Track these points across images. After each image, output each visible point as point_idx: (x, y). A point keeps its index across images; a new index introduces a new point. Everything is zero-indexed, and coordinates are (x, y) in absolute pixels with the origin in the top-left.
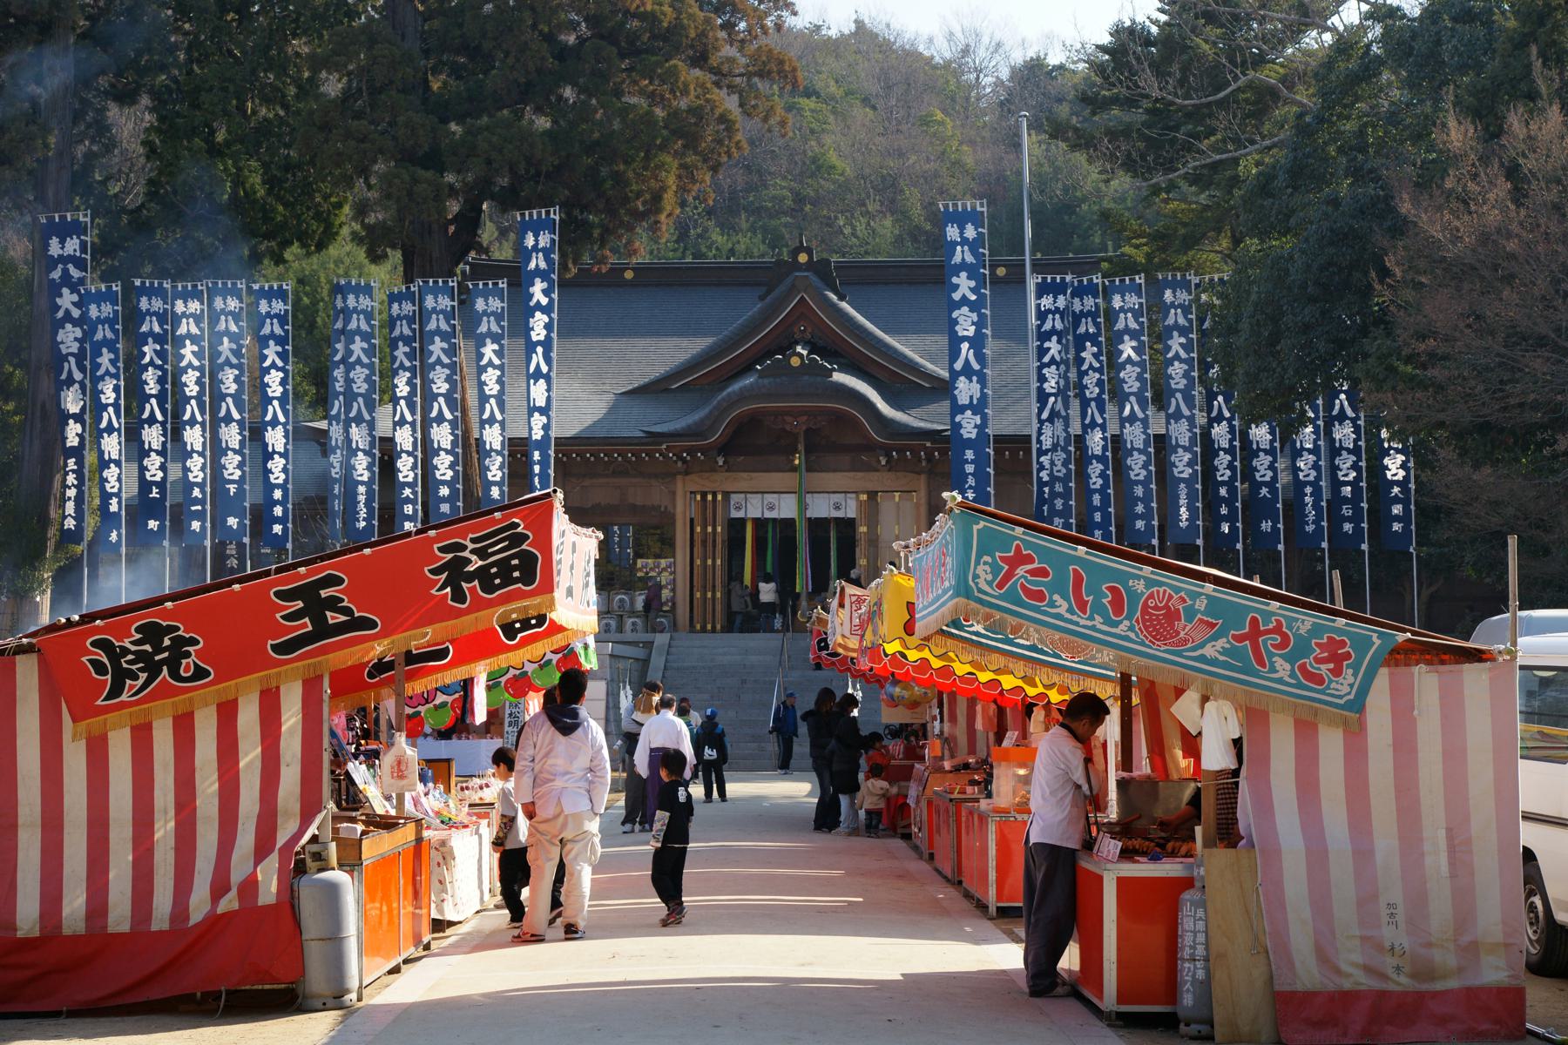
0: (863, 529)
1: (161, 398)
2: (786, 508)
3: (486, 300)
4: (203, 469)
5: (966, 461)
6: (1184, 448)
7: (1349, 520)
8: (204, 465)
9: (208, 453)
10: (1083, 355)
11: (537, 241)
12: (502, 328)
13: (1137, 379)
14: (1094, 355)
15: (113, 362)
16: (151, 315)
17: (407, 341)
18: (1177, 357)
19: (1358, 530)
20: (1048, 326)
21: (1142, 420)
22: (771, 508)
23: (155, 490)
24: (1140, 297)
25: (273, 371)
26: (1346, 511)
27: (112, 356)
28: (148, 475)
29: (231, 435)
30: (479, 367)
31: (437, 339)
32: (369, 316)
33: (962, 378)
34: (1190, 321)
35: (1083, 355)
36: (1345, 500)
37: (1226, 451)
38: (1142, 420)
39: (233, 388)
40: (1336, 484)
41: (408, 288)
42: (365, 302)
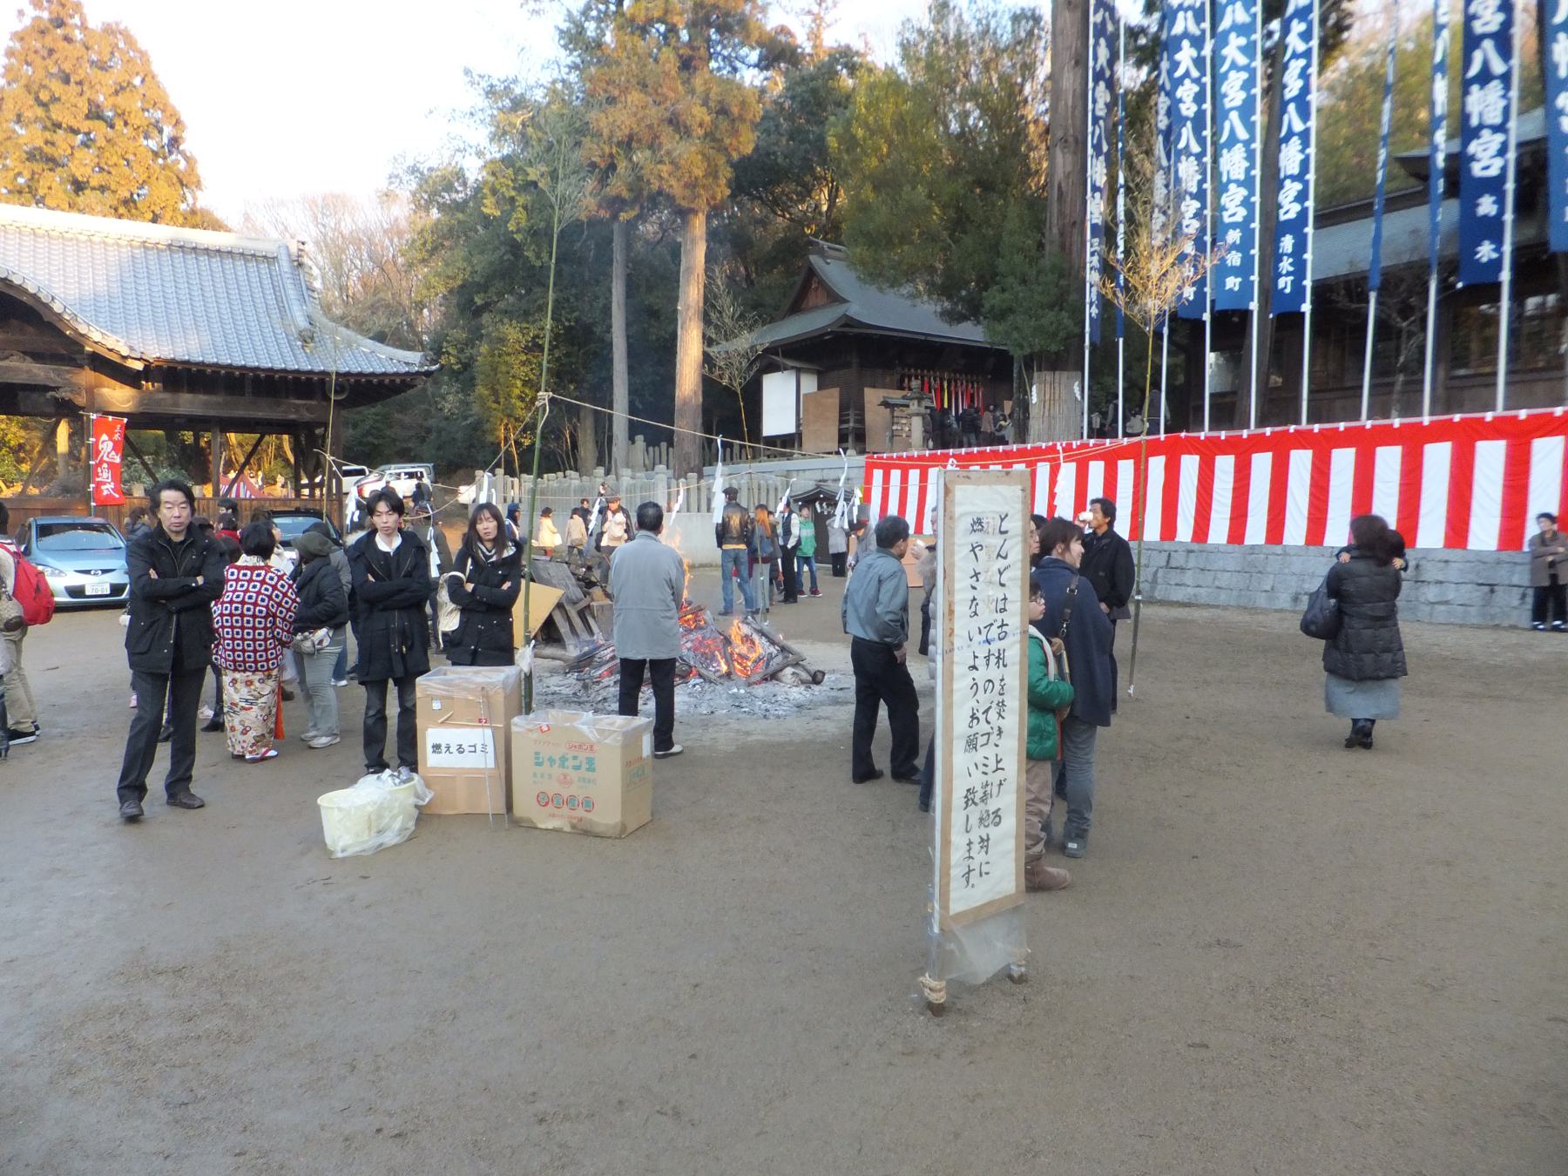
19: (1246, 286)
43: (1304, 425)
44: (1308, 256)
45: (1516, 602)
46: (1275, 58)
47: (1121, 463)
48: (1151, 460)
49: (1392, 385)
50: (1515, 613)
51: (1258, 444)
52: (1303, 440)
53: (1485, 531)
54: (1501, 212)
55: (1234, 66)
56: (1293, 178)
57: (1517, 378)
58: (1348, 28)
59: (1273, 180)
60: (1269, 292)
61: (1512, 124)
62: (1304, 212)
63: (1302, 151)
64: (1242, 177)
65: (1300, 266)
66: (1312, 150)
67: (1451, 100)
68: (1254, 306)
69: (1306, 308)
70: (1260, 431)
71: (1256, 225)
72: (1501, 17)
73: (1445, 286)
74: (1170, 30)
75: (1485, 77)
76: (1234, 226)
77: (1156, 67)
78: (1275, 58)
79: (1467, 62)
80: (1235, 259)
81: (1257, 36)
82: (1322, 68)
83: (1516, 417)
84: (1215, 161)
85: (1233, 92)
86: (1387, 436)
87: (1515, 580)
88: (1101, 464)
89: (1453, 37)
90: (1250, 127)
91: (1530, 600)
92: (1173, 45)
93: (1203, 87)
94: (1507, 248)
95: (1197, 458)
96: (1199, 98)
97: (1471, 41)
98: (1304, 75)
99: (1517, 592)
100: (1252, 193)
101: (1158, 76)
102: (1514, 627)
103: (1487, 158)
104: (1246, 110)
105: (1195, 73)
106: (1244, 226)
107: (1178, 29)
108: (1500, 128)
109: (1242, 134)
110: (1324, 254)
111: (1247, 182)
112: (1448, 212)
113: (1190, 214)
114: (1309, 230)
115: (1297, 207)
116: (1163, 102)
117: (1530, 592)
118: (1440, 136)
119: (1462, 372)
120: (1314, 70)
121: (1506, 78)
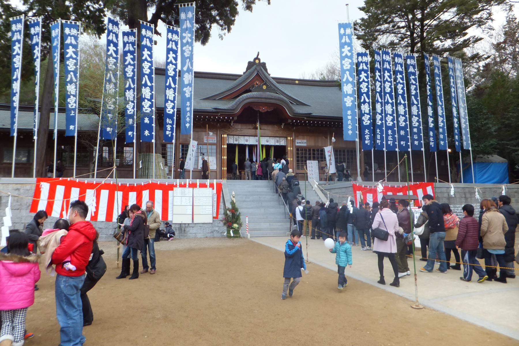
0: (289, 148)
2: (251, 141)
4: (133, 108)
5: (348, 115)
7: (416, 140)
8: (134, 106)
9: (135, 101)
10: (126, 58)
11: (345, 32)
12: (368, 67)
14: (131, 59)
19: (420, 144)
20: (127, 49)
21: (150, 87)
23: (73, 112)
24: (135, 38)
25: (129, 66)
26: (416, 137)
29: (401, 110)
30: (124, 65)
31: (70, 47)
33: (187, 74)
34: (135, 49)
35: (126, 58)
36: (415, 133)
38: (150, 87)
40: (411, 127)
41: (132, 31)
48: (144, 192)
55: (364, 81)
57: (79, 168)
59: (411, 116)
62: (174, 111)
63: (151, 92)
68: (384, 149)
71: (421, 127)
84: (385, 107)
90: (417, 101)
95: (108, 191)
100: (420, 119)
111: (418, 116)
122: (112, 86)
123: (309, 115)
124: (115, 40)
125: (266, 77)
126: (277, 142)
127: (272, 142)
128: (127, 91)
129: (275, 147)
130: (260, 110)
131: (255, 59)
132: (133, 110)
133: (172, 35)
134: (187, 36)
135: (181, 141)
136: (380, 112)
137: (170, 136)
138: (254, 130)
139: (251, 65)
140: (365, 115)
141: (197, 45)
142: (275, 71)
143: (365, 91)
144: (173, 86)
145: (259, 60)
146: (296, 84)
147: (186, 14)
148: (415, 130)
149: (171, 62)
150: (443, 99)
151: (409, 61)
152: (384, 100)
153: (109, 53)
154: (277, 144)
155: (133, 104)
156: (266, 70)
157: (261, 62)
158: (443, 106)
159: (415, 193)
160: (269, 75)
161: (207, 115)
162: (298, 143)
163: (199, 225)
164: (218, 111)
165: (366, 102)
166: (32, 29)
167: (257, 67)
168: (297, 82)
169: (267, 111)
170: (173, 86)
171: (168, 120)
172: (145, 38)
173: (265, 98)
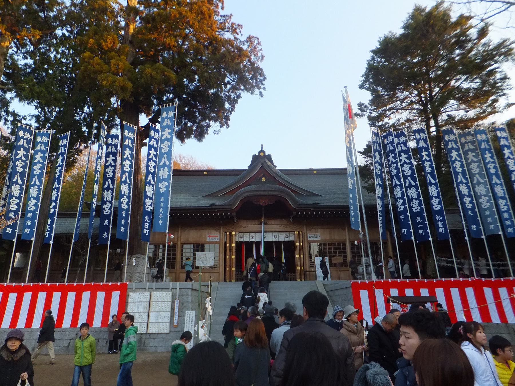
0: (297, 244)
1: (464, 173)
2: (257, 237)
3: (42, 138)
6: (415, 199)
11: (167, 115)
13: (410, 169)
14: (113, 160)
15: (492, 157)
16: (451, 141)
17: (472, 151)
18: (472, 161)
19: (32, 232)
21: (414, 186)
22: (252, 238)
25: (110, 167)
27: (490, 155)
28: (414, 209)
32: (456, 142)
34: (65, 150)
37: (468, 196)
39: (477, 170)
42: (452, 137)
43: (458, 278)
44: (54, 226)
45: (104, 345)
46: (53, 163)
47: (99, 293)
49: (77, 270)
50: (104, 348)
51: (27, 289)
52: (43, 288)
53: (97, 323)
54: (109, 224)
56: (400, 198)
58: (76, 163)
59: (28, 198)
60: (40, 234)
61: (113, 202)
62: (55, 211)
63: (416, 191)
64: (18, 196)
65: (51, 228)
66: (59, 194)
67: (99, 191)
69: (51, 242)
70: (11, 284)
71: (38, 212)
72: (112, 174)
73: (94, 243)
74: (17, 143)
75: (108, 189)
76: (31, 212)
77: (11, 152)
78: (53, 163)
79: (104, 184)
80: (29, 223)
81: (47, 155)
82: (66, 171)
83: (510, 280)
85: (37, 169)
86: (71, 288)
87: (105, 337)
88: (103, 293)
89: (100, 174)
90: (41, 181)
91: (108, 343)
92: (19, 148)
93: (132, 163)
94: (110, 235)
96: (24, 167)
97: (105, 179)
98: (60, 172)
99: (105, 341)
101: (12, 155)
102: (103, 353)
103: (107, 209)
104: (40, 176)
105: (459, 159)
106: (34, 212)
107: (21, 143)
108: (110, 202)
109: (38, 183)
110: (55, 227)
111: (37, 198)
112: (96, 222)
113: (467, 202)
114: (55, 218)
115: (403, 207)
116: (11, 164)
117: (108, 341)
118: (95, 200)
119: (99, 269)
120: (63, 171)
121: (113, 190)
122: (413, 189)
123: (316, 206)
124: (155, 145)
125: (271, 169)
126: (287, 237)
127: (281, 238)
128: (106, 191)
129: (285, 243)
130: (261, 204)
131: (260, 152)
132: (110, 211)
133: (419, 134)
134: (166, 134)
135: (182, 240)
136: (4, 197)
137: (147, 235)
138: (259, 226)
139: (255, 158)
140: (414, 200)
141: (176, 142)
142: (282, 162)
143: (111, 176)
144: (413, 184)
145: (264, 152)
146: (314, 174)
147: (167, 113)
148: (30, 215)
149: (405, 163)
150: (132, 178)
151: (39, 139)
152: (405, 183)
153: (150, 157)
154: (286, 239)
155: (110, 205)
156: (272, 162)
157: (266, 154)
158: (132, 186)
159: (432, 294)
160: (276, 167)
161: (199, 212)
162: (310, 237)
163: (161, 336)
164: (214, 207)
165: (413, 186)
166: (61, 141)
167: (262, 161)
168: (315, 172)
169: (269, 204)
170: (413, 184)
171: (437, 217)
172: (450, 143)
173: (265, 191)
